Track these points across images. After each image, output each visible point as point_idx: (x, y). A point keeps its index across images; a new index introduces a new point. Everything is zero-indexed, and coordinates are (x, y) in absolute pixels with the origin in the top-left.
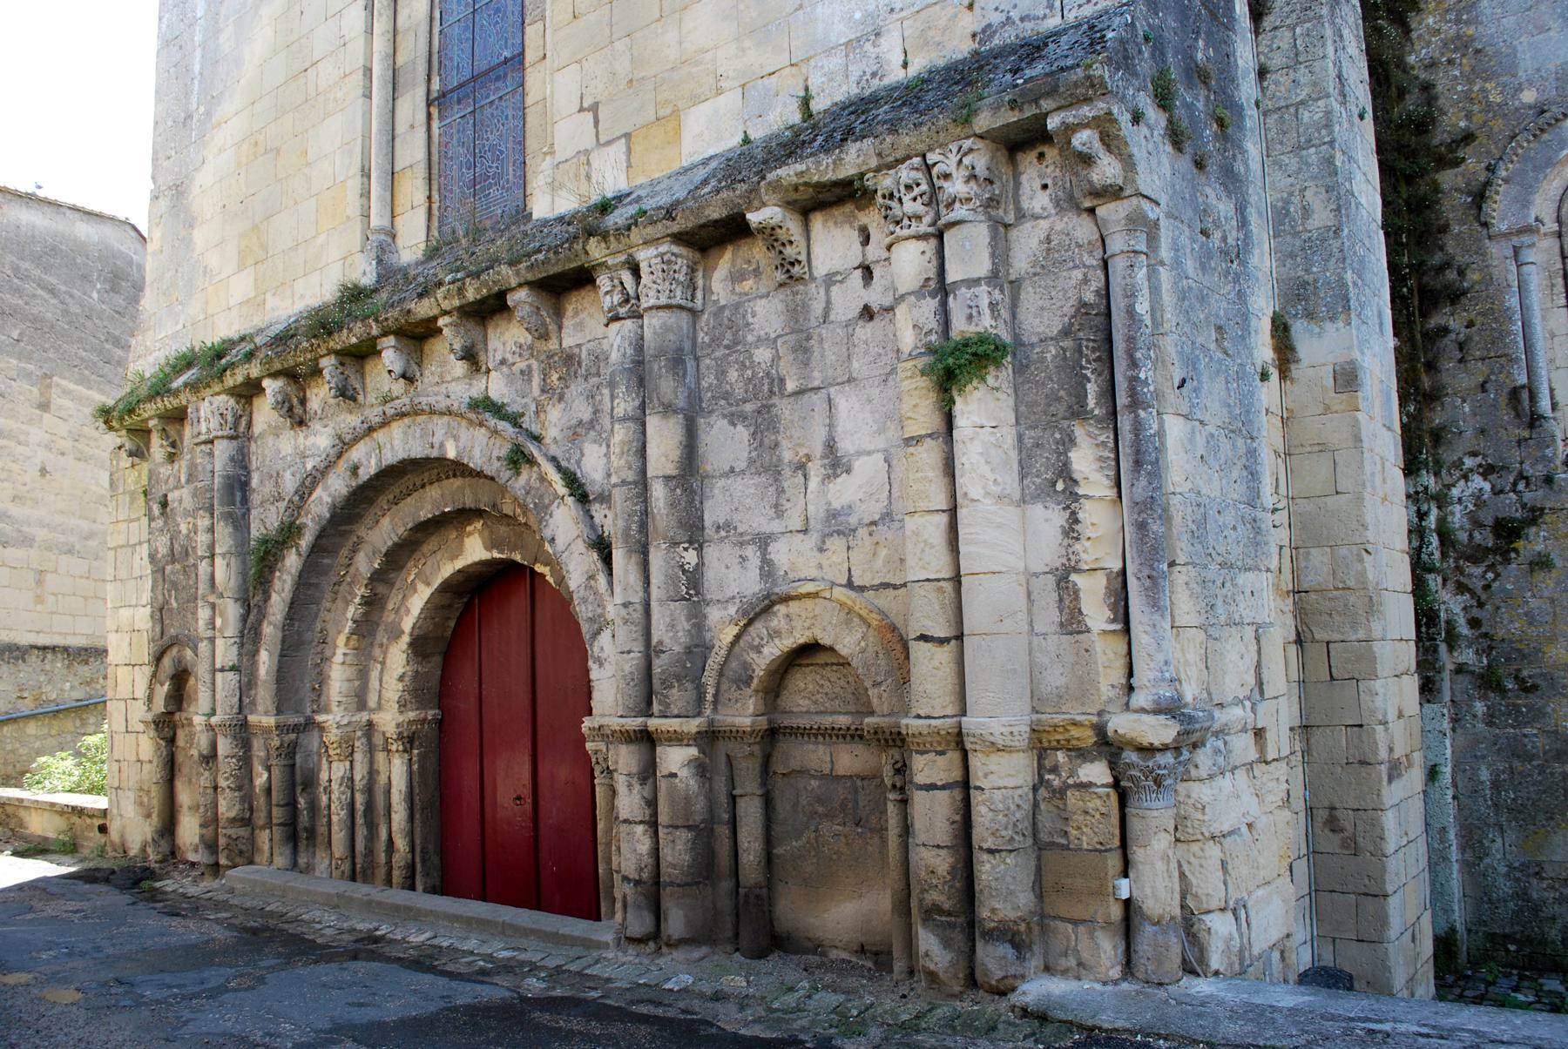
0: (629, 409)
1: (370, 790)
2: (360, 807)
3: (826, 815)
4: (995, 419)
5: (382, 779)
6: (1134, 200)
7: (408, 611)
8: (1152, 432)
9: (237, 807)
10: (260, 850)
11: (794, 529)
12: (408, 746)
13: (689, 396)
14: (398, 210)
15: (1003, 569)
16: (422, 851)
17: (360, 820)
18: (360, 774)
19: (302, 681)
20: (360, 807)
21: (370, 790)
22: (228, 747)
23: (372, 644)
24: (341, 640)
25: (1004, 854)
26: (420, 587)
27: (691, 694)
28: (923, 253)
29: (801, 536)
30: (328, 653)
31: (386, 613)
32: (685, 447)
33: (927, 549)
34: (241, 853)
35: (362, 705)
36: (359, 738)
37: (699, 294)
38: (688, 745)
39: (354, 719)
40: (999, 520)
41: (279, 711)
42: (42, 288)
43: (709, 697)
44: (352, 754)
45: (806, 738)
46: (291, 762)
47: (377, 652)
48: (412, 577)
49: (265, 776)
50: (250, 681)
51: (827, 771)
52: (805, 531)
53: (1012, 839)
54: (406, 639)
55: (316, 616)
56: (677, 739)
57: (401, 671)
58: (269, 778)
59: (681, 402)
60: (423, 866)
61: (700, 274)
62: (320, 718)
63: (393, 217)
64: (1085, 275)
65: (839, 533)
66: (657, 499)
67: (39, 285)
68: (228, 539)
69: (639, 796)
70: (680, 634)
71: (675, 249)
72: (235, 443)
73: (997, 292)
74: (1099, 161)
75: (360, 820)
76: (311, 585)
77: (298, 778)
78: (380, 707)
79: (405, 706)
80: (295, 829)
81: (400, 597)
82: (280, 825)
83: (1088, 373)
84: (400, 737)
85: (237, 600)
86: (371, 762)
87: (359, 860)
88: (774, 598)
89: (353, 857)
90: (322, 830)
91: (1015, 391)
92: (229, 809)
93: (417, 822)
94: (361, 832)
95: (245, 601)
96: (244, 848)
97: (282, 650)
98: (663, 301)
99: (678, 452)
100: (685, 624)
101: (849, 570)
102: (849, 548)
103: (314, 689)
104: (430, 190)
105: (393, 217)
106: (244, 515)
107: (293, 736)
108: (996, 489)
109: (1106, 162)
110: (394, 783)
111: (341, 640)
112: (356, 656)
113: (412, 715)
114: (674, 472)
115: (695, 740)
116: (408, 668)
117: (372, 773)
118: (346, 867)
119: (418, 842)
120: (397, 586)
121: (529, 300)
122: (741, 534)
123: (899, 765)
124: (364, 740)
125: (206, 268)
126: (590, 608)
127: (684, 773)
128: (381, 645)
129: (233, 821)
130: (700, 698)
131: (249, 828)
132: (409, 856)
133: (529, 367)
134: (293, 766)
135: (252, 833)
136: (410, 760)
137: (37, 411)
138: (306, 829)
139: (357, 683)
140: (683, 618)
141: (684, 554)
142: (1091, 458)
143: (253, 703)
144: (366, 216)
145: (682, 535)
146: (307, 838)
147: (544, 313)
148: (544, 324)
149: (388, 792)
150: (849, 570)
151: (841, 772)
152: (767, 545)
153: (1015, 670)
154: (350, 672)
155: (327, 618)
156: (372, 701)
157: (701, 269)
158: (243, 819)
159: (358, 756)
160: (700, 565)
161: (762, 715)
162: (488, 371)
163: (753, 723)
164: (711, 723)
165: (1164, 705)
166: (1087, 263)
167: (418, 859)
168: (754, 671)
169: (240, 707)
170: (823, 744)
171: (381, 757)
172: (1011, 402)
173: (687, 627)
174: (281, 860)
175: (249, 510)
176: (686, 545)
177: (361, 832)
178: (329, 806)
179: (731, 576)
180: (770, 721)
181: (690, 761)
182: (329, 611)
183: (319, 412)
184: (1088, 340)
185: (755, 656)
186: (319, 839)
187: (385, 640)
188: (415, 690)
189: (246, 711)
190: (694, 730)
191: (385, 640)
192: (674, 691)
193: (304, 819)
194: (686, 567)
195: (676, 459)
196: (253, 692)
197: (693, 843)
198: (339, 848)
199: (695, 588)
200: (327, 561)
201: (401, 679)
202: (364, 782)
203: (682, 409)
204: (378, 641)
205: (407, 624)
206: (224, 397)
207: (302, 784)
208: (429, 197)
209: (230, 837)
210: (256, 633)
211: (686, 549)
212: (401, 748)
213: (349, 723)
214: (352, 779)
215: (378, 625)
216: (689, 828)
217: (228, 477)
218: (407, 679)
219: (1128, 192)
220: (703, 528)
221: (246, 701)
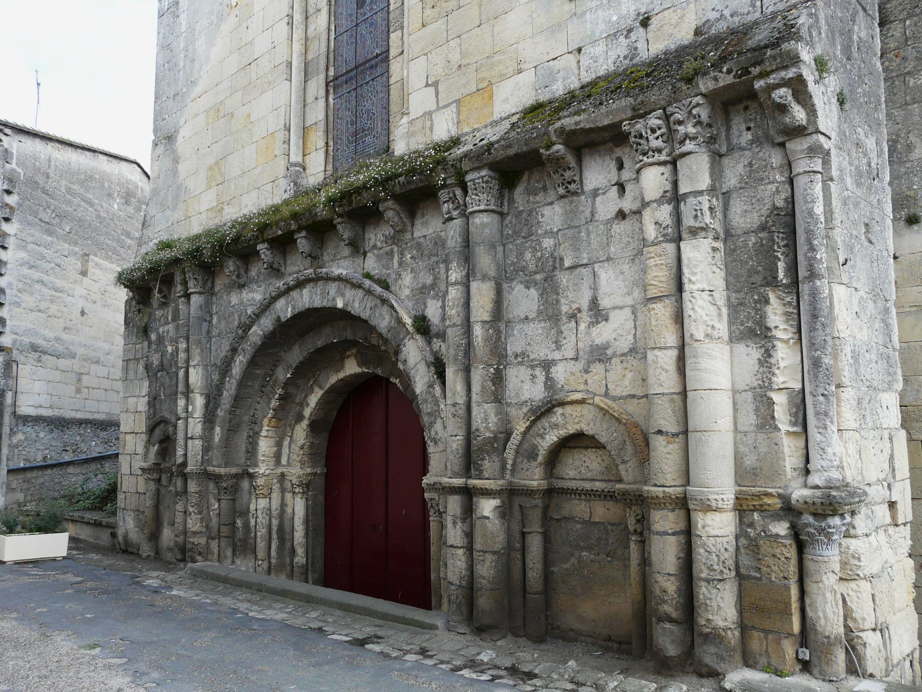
0: (459, 277)
3: (586, 548)
5: (289, 510)
7: (308, 405)
11: (568, 357)
18: (275, 504)
20: (275, 528)
23: (285, 425)
28: (663, 174)
29: (573, 362)
42: (84, 201)
43: (509, 467)
45: (573, 496)
46: (232, 498)
51: (587, 519)
52: (576, 359)
57: (303, 442)
65: (600, 360)
66: (477, 336)
70: (490, 425)
75: (274, 536)
81: (303, 395)
85: (202, 394)
86: (283, 498)
88: (554, 402)
101: (606, 386)
102: (606, 371)
113: (309, 470)
117: (283, 505)
122: (532, 360)
123: (640, 517)
126: (429, 406)
128: (290, 426)
137: (80, 276)
140: (492, 415)
150: (606, 386)
151: (597, 520)
152: (550, 367)
154: (272, 442)
166: (779, 180)
167: (310, 562)
168: (539, 450)
170: (585, 500)
171: (289, 496)
173: (495, 420)
179: (525, 387)
185: (540, 441)
193: (240, 534)
195: (490, 310)
205: (307, 412)
208: (327, 143)
209: (193, 543)
214: (270, 509)
216: (494, 553)
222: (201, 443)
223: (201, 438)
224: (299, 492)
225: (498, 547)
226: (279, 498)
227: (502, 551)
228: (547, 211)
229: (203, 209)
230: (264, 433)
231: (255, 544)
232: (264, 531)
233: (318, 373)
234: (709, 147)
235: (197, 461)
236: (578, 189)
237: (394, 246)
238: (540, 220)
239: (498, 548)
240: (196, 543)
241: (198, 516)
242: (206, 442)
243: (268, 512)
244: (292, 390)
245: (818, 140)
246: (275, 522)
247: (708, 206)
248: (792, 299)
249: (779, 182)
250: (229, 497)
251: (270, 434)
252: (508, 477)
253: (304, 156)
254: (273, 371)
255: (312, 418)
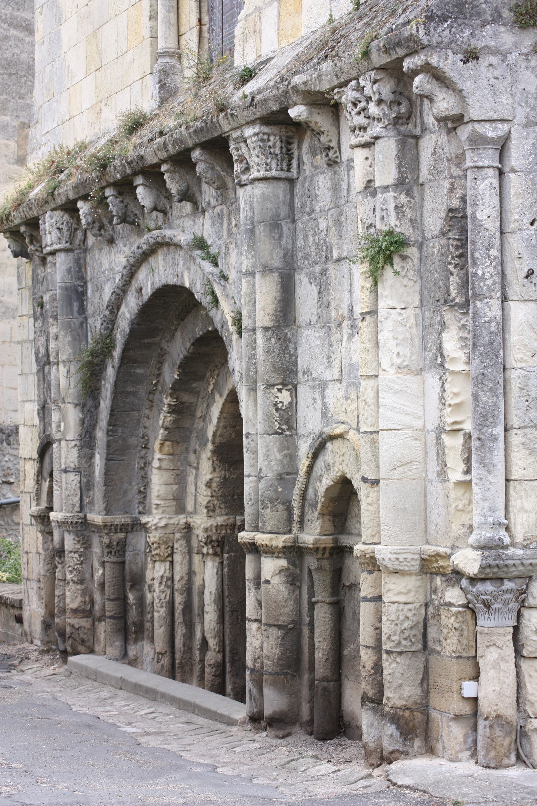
0: (250, 265)
1: (188, 590)
2: (179, 608)
4: (403, 302)
5: (197, 581)
6: (470, 125)
8: (487, 319)
9: (79, 599)
10: (99, 640)
12: (218, 550)
13: (285, 256)
14: (183, 30)
15: (398, 428)
16: (231, 651)
17: (179, 617)
18: (180, 571)
19: (130, 483)
20: (179, 608)
21: (188, 590)
22: (72, 542)
23: (187, 449)
24: (157, 445)
25: (395, 655)
26: (217, 397)
27: (282, 514)
28: (367, 158)
30: (150, 458)
31: (197, 421)
32: (280, 301)
33: (366, 407)
34: (83, 642)
35: (181, 509)
36: (178, 540)
37: (295, 163)
38: (278, 557)
39: (172, 522)
40: (396, 387)
41: (108, 511)
42: (15, 28)
43: (296, 518)
44: (172, 554)
46: (120, 560)
47: (192, 458)
48: (211, 387)
49: (101, 572)
50: (88, 481)
52: (340, 381)
53: (399, 643)
54: (210, 446)
55: (139, 422)
56: (270, 551)
57: (209, 476)
58: (103, 574)
59: (277, 263)
60: (231, 666)
61: (295, 146)
62: (144, 519)
63: (179, 36)
64: (452, 184)
67: (11, 24)
68: (67, 347)
69: (254, 599)
70: (273, 463)
71: (265, 129)
72: (71, 255)
73: (402, 196)
74: (435, 98)
75: (179, 617)
76: (129, 393)
77: (128, 578)
78: (195, 512)
79: (214, 511)
80: (125, 623)
81: (205, 405)
82: (110, 617)
83: (451, 267)
84: (209, 542)
85: (76, 405)
87: (178, 656)
89: (173, 653)
90: (147, 625)
91: (421, 278)
92: (73, 600)
93: (227, 624)
94: (180, 631)
95: (82, 406)
96: (85, 637)
97: (108, 454)
98: (262, 173)
99: (273, 307)
100: (277, 454)
103: (140, 492)
104: (200, 12)
105: (179, 36)
106: (81, 324)
107: (121, 535)
108: (397, 361)
109: (440, 98)
110: (207, 584)
111: (157, 445)
112: (172, 461)
113: (220, 520)
114: (269, 324)
115: (284, 553)
116: (216, 475)
117: (191, 573)
118: (166, 661)
119: (227, 642)
120: (201, 395)
121: (202, 158)
124: (183, 542)
125: (69, 67)
127: (276, 581)
128: (195, 452)
129: (75, 611)
130: (290, 519)
131: (90, 620)
132: (220, 656)
133: (222, 210)
134: (124, 563)
135: (93, 624)
136: (222, 563)
137: (16, 167)
138: (135, 624)
139: (175, 487)
140: (275, 450)
141: (279, 394)
142: (456, 338)
143: (92, 503)
144: (154, 37)
145: (276, 379)
146: (136, 632)
147: (218, 168)
148: (219, 177)
149: (202, 593)
153: (405, 509)
154: (167, 476)
155: (147, 424)
156: (190, 507)
157: (296, 142)
158: (84, 611)
159: (177, 558)
160: (293, 406)
161: (331, 535)
162: (204, 211)
163: (316, 542)
164: (296, 540)
165: (482, 544)
166: (454, 174)
167: (227, 660)
169: (81, 507)
171: (197, 558)
172: (418, 287)
173: (279, 456)
174: (114, 650)
175: (86, 319)
176: (280, 387)
177: (180, 631)
178: (153, 603)
180: (336, 541)
181: (281, 571)
182: (148, 418)
183: (121, 231)
184: (454, 239)
186: (146, 633)
187: (197, 447)
188: (224, 496)
189: (87, 510)
190: (281, 545)
191: (197, 447)
192: (268, 511)
193: (133, 613)
194: (280, 406)
195: (271, 312)
196: (91, 493)
197: (282, 640)
198: (160, 644)
199: (287, 423)
200: (139, 371)
201: (209, 484)
202: (183, 582)
203: (278, 269)
204: (191, 449)
205: (210, 434)
206: (58, 213)
207: (131, 581)
208: (200, 20)
209: (73, 626)
210: (91, 437)
211: (280, 390)
212: (211, 551)
213: (166, 526)
214: (172, 579)
215: (191, 432)
216: (279, 627)
217: (66, 289)
218: (214, 485)
219: (466, 119)
220: (297, 373)
221: (86, 500)
222: (78, 478)
223: (77, 470)
224: (208, 554)
225: (284, 620)
226: (186, 561)
227: (291, 626)
228: (321, 178)
229: (84, 108)
230: (156, 464)
231: (153, 629)
232: (163, 610)
233: (216, 372)
234: (398, 129)
235: (73, 505)
236: (337, 157)
237: (224, 206)
238: (317, 192)
239: (284, 621)
240: (77, 626)
241: (79, 587)
242: (85, 476)
243: (169, 583)
244: (186, 397)
245: (474, 131)
246: (179, 599)
247: (394, 204)
248: (467, 321)
249: (455, 177)
250: (115, 559)
251: (165, 464)
252: (295, 530)
253: (179, 36)
254: (159, 369)
255: (218, 440)
